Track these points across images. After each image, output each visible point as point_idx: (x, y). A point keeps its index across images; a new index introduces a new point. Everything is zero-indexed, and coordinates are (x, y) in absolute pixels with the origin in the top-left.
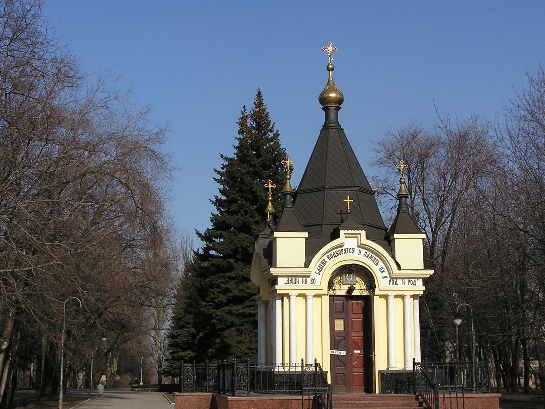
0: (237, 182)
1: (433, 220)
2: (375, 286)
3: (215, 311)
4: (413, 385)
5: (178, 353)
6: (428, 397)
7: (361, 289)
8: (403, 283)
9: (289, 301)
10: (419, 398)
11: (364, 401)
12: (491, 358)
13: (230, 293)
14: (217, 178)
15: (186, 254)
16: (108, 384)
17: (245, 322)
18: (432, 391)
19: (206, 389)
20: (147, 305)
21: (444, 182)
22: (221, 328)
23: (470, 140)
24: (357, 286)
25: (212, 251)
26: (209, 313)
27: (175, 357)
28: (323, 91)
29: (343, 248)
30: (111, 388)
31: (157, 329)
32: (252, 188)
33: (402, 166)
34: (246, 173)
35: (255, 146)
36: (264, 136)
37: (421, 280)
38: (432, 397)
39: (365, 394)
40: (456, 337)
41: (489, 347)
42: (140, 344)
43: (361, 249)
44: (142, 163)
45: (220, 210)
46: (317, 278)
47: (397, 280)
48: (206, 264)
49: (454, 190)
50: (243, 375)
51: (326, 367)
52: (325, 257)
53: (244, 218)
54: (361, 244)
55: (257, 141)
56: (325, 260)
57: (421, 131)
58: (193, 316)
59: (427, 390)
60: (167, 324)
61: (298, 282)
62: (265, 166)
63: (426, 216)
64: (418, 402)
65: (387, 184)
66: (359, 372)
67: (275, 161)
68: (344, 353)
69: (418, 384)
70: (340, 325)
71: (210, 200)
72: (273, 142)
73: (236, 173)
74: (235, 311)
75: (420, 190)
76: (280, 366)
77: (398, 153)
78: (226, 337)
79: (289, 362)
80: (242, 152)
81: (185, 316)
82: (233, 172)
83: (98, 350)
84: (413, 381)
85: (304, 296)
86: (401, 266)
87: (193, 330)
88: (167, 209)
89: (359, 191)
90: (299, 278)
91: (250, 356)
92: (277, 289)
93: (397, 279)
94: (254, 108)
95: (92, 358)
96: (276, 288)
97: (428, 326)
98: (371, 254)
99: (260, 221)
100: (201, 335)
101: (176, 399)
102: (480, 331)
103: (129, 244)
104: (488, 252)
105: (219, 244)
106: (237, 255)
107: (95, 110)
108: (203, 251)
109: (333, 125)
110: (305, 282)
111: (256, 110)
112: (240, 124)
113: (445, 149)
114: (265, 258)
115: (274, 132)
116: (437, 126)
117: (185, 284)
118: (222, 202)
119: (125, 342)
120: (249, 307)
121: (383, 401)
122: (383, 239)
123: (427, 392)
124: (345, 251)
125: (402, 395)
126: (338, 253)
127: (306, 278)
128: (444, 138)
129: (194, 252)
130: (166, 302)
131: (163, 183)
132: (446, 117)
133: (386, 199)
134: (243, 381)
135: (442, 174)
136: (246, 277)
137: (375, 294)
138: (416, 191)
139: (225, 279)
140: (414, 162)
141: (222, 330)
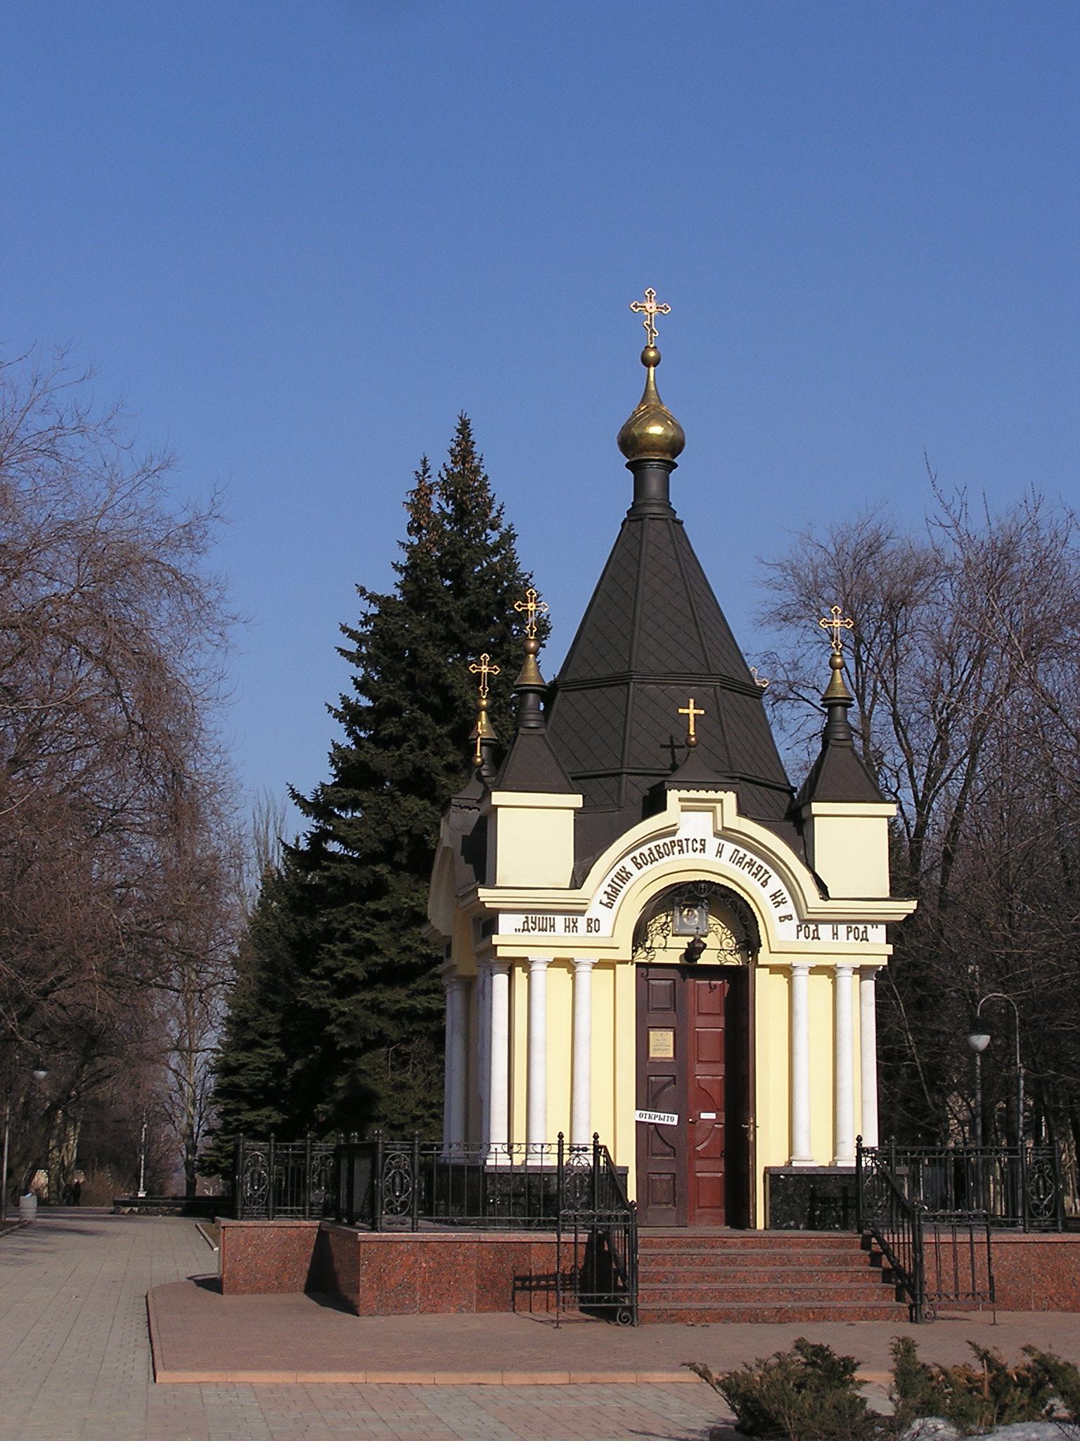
0: (402, 658)
1: (920, 772)
2: (760, 941)
3: (336, 1001)
4: (856, 1207)
5: (240, 1114)
6: (896, 1241)
7: (723, 950)
8: (834, 934)
9: (529, 978)
10: (870, 1243)
11: (724, 1248)
12: (1067, 1141)
13: (376, 956)
14: (347, 650)
15: (266, 853)
16: (53, 1195)
17: (414, 1032)
18: (906, 1225)
19: (303, 1212)
20: (157, 986)
21: (949, 670)
22: (352, 1047)
23: (1022, 561)
24: (711, 941)
25: (331, 842)
26: (321, 1009)
27: (230, 1123)
28: (630, 420)
29: (675, 838)
30: (58, 1205)
31: (185, 1050)
32: (439, 676)
33: (837, 623)
34: (426, 636)
35: (451, 565)
36: (475, 538)
37: (883, 928)
38: (906, 1241)
39: (726, 1230)
40: (975, 1083)
41: (1061, 1110)
42: (139, 1087)
43: (723, 842)
44: (148, 603)
45: (356, 733)
46: (606, 916)
47: (817, 926)
48: (312, 878)
49: (977, 694)
50: (400, 1173)
51: (625, 1156)
52: (627, 863)
53: (417, 757)
54: (723, 828)
55: (455, 553)
56: (627, 870)
57: (892, 536)
58: (280, 1016)
59: (892, 1221)
60: (212, 1038)
61: (554, 926)
62: (476, 620)
63: (902, 759)
64: (869, 1253)
65: (799, 675)
66: (712, 1172)
67: (502, 604)
68: (673, 1120)
69: (870, 1206)
70: (662, 1044)
71: (329, 707)
72: (499, 557)
73: (397, 636)
74: (387, 1004)
75: (887, 692)
76: (499, 1150)
77: (829, 593)
78: (363, 1072)
79: (524, 1142)
80: (416, 580)
81: (259, 1014)
82: (390, 634)
83: (25, 1104)
84: (857, 1198)
85: (570, 965)
86: (829, 890)
87: (280, 1054)
88: (211, 728)
90: (557, 917)
91: (426, 1125)
92: (496, 946)
93: (817, 922)
94: (450, 465)
95: (7, 1123)
96: (494, 942)
97: (902, 1052)
98: (750, 856)
99: (461, 766)
100: (298, 1065)
101: (222, 1235)
102: (1038, 1065)
103: (110, 821)
104: (1063, 857)
105: (350, 825)
106: (397, 854)
107: (23, 460)
108: (308, 844)
109: (656, 510)
111: (456, 470)
112: (411, 506)
113: (955, 584)
114: (467, 862)
115: (501, 530)
116: (935, 521)
117: (259, 933)
118: (360, 713)
119: (98, 1081)
120: (426, 992)
121: (776, 1250)
122: (783, 816)
123: (892, 1226)
124: (681, 846)
125: (826, 1234)
126: (662, 850)
127: (575, 917)
128: (952, 554)
129: (284, 844)
130: (209, 977)
131: (201, 660)
132: (957, 498)
133: (796, 713)
134: (401, 1192)
135: (946, 649)
136: (420, 913)
137: (760, 963)
138: (875, 693)
139: (363, 918)
140: (872, 616)
141: (354, 1053)
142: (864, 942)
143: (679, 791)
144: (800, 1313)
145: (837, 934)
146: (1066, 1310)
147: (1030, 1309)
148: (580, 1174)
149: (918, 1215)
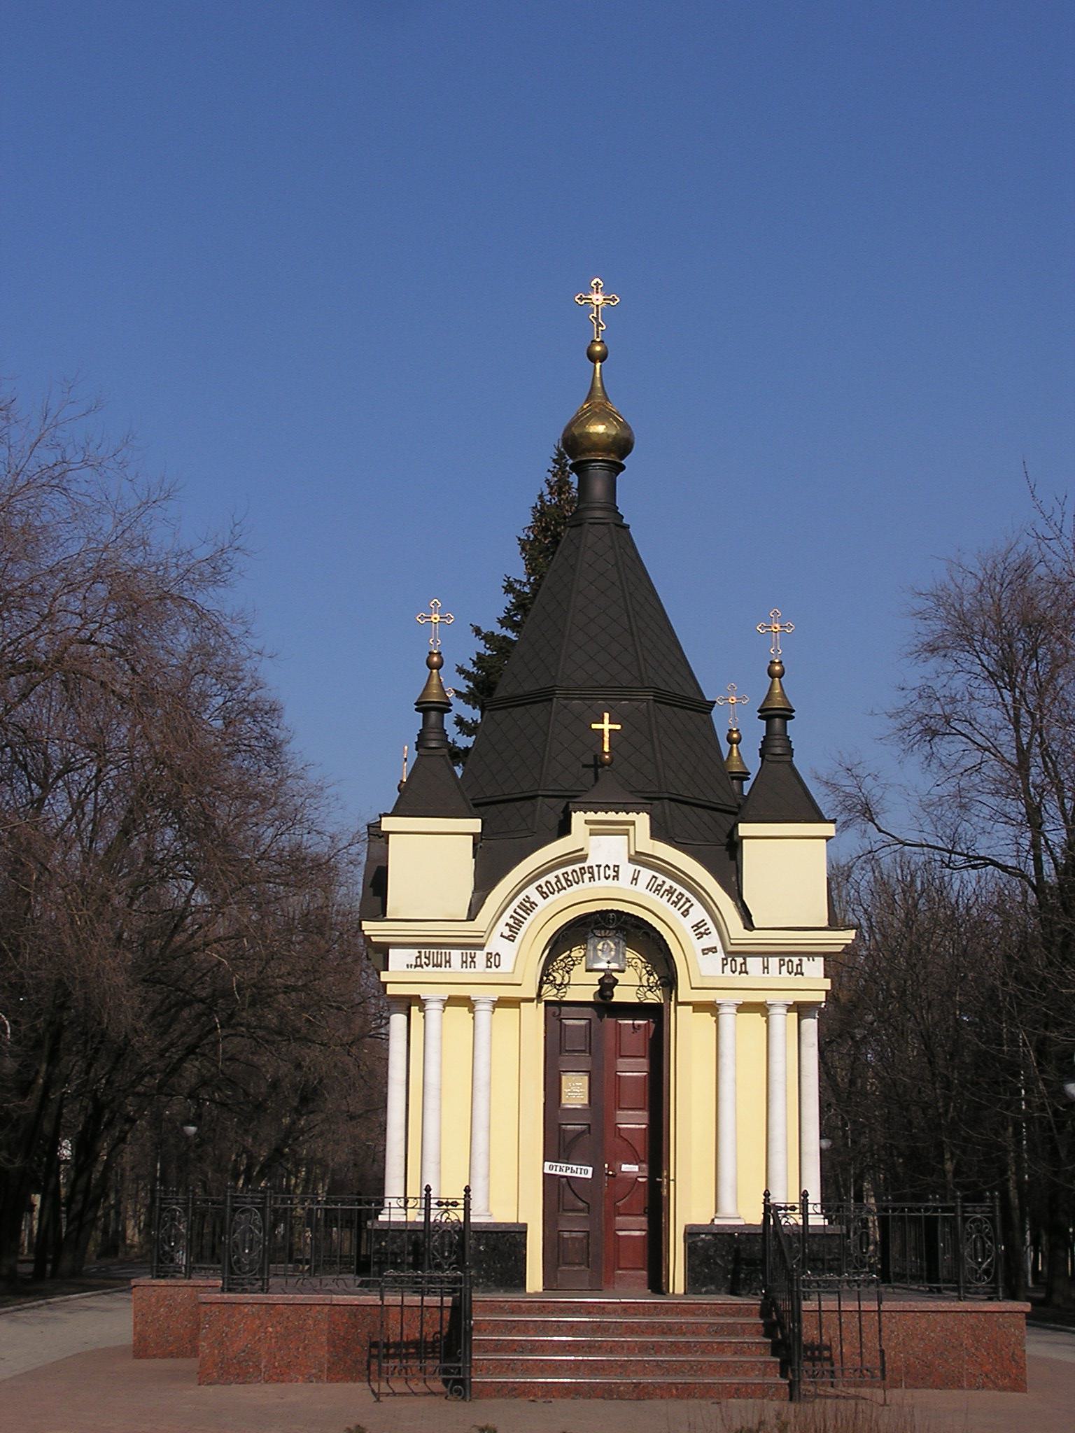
8: (764, 968)
29: (585, 865)
43: (639, 868)
47: (745, 959)
56: (531, 900)
61: (449, 962)
68: (588, 1172)
70: (575, 1091)
85: (468, 1003)
86: (753, 918)
93: (745, 955)
109: (598, 514)
110: (469, 962)
124: (592, 873)
126: (570, 878)
127: (473, 952)
142: (743, 975)
143: (585, 813)
144: (661, 1388)
145: (767, 968)
146: (1005, 1389)
147: (962, 1387)
148: (449, 1231)
149: (797, 1280)
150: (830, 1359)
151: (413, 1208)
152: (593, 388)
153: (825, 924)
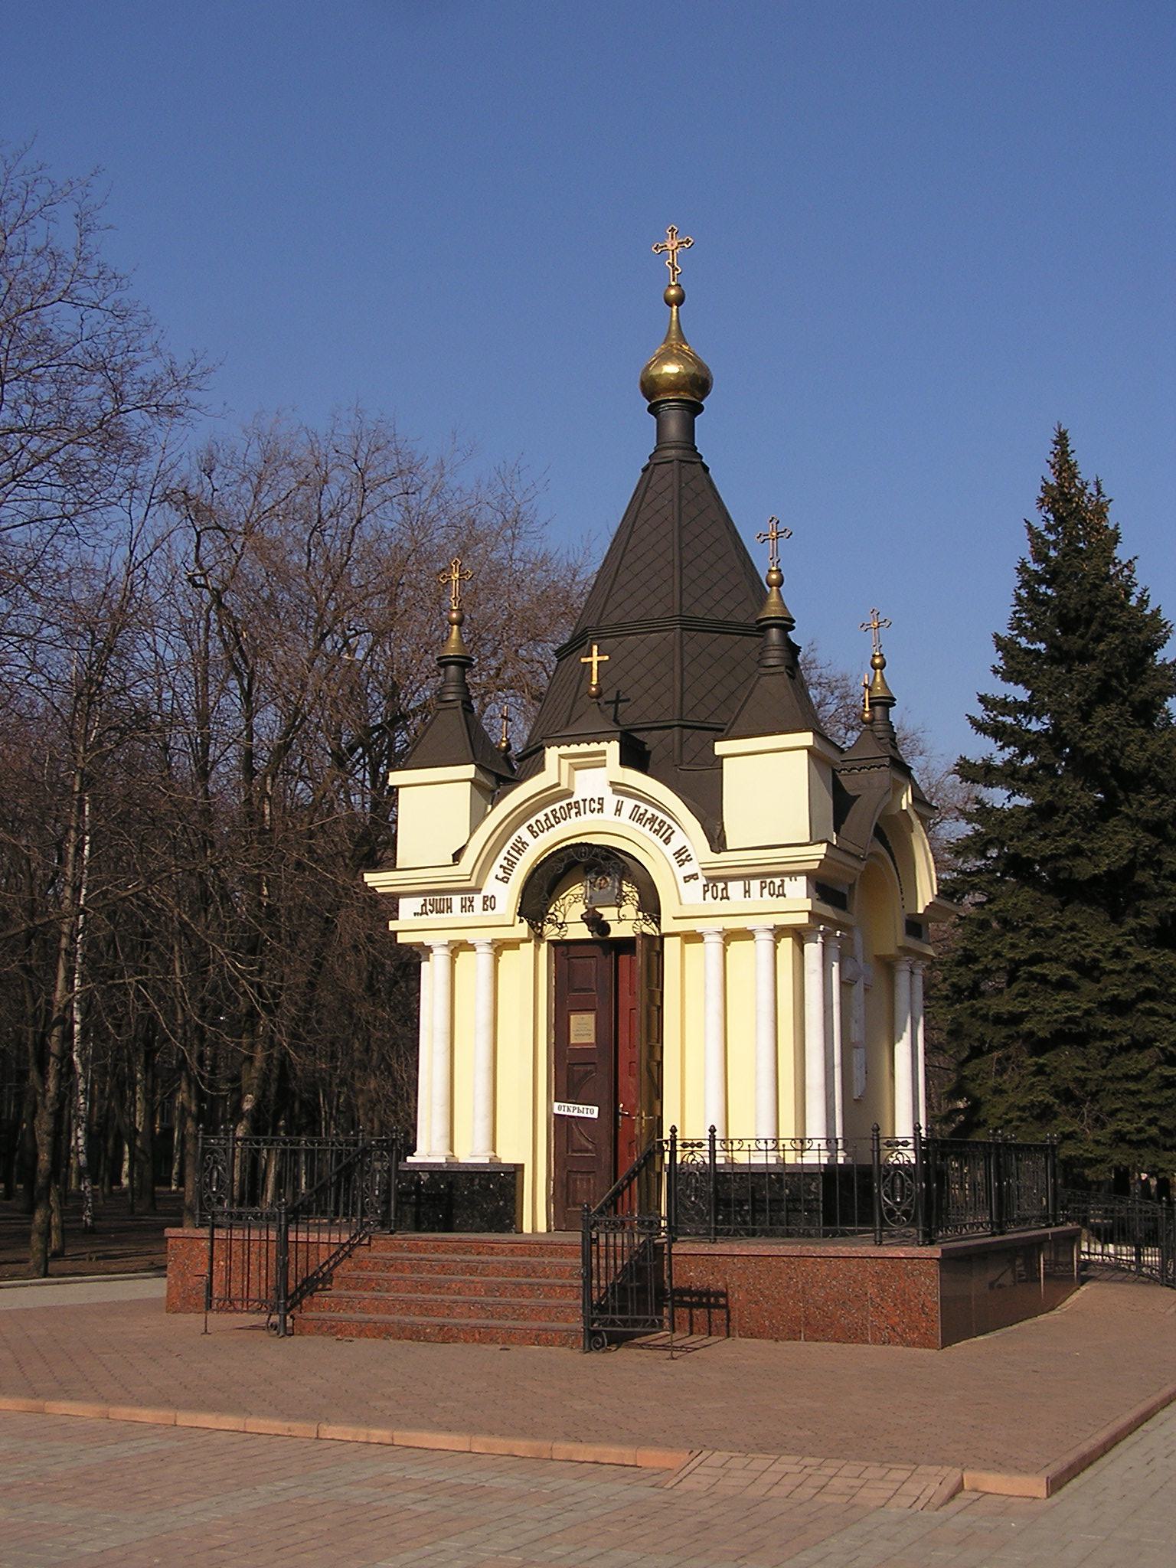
8: (746, 892)
29: (572, 800)
37: (803, 880)
43: (621, 798)
70: (583, 1029)
89: (683, 629)
90: (453, 897)
93: (726, 879)
124: (579, 808)
126: (558, 815)
127: (471, 896)
142: (780, 898)
144: (465, 1332)
146: (912, 1344)
147: (867, 1342)
150: (725, 1306)
151: (739, 1150)
152: (669, 332)
153: (807, 839)
